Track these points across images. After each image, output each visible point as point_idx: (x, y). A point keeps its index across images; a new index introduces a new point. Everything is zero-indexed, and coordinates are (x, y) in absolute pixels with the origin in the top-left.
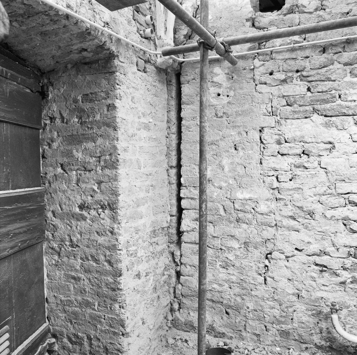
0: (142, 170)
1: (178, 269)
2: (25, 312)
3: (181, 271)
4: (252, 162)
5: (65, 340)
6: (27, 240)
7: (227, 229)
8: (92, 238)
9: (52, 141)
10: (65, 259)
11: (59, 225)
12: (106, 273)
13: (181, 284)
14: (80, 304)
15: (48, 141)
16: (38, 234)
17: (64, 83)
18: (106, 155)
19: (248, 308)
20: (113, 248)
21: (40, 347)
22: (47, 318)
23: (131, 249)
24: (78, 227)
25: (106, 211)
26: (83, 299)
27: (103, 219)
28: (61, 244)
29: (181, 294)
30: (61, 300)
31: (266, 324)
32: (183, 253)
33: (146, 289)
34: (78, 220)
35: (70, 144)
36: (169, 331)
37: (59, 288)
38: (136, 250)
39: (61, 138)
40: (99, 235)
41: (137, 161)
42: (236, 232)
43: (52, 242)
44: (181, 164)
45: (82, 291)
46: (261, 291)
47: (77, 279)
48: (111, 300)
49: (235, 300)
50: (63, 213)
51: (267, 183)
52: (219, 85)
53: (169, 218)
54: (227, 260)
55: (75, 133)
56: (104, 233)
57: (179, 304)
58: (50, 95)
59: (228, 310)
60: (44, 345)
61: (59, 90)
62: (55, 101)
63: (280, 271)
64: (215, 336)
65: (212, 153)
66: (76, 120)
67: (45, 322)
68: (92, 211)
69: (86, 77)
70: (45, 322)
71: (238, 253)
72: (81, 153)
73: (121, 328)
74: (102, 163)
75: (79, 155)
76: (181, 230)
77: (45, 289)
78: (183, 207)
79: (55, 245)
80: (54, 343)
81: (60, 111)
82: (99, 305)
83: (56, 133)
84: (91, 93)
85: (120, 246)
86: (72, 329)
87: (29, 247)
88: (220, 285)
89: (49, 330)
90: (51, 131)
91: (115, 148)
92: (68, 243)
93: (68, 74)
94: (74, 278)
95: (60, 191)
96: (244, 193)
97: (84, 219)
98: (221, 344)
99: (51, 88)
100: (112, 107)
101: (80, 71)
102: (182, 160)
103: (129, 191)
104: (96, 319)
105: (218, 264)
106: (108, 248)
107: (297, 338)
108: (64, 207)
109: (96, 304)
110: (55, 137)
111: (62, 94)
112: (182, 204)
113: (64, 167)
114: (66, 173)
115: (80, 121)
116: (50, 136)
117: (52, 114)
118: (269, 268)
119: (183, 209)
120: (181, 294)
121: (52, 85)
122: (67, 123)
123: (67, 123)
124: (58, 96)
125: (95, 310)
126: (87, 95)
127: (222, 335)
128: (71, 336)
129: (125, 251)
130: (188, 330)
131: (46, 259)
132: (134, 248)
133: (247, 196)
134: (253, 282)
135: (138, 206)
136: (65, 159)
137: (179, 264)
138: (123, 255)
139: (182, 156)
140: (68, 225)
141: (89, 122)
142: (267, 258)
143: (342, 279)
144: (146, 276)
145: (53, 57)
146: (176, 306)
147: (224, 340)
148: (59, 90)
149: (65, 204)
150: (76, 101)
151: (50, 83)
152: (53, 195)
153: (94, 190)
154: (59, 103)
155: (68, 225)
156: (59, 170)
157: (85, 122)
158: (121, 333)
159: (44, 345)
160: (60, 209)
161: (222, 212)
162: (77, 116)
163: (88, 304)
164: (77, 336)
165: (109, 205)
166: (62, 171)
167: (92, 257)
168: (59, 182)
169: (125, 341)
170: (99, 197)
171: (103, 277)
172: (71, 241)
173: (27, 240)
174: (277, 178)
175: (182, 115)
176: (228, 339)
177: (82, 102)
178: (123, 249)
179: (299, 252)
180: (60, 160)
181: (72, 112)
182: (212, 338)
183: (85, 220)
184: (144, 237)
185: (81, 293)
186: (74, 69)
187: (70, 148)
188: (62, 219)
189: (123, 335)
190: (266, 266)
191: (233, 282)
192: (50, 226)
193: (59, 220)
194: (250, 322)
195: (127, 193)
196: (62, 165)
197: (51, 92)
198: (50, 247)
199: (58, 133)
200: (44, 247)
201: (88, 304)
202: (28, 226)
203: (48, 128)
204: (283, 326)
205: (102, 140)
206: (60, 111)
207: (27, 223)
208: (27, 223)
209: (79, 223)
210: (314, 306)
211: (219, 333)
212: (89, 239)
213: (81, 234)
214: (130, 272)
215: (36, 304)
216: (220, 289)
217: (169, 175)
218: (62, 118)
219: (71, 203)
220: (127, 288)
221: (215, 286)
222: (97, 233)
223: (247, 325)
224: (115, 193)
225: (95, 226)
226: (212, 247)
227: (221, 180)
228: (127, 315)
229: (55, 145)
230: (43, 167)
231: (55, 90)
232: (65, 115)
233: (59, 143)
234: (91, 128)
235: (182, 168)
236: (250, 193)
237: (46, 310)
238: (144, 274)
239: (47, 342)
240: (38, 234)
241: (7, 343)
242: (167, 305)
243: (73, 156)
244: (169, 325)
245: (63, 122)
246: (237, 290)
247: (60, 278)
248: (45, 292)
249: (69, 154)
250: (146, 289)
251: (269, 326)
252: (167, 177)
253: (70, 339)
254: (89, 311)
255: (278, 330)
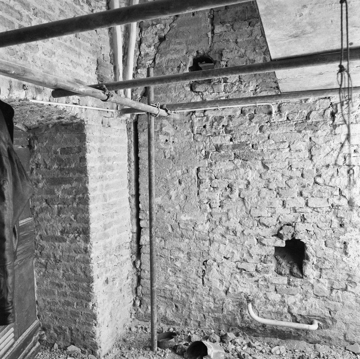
0: (108, 202)
1: (139, 274)
2: (23, 312)
3: (141, 275)
4: (192, 193)
5: (52, 332)
6: (23, 259)
7: (174, 243)
8: (71, 254)
9: (39, 183)
10: (51, 271)
11: (45, 245)
12: (83, 281)
13: (142, 286)
14: (63, 304)
15: (35, 182)
16: (30, 253)
17: (46, 138)
18: (79, 194)
19: (191, 302)
20: (88, 262)
21: (34, 338)
22: (38, 315)
23: (100, 262)
24: (60, 247)
25: (81, 236)
26: (65, 301)
27: (79, 241)
28: (47, 260)
29: (142, 293)
30: (48, 302)
31: (204, 313)
32: (142, 261)
33: (113, 291)
34: (60, 242)
35: (52, 184)
36: (133, 322)
37: (47, 292)
38: (105, 262)
39: (45, 180)
40: (76, 253)
41: (104, 196)
42: (182, 245)
43: (40, 258)
44: (140, 193)
45: (65, 295)
46: (200, 290)
47: (60, 286)
48: (86, 300)
49: (182, 296)
50: (49, 236)
51: (202, 209)
52: (167, 134)
53: (131, 234)
54: (175, 267)
55: (55, 177)
56: (80, 252)
57: (141, 301)
58: (36, 147)
59: (177, 304)
60: (37, 336)
61: (42, 143)
62: (39, 152)
63: (214, 275)
64: (168, 324)
65: (162, 185)
66: (56, 167)
67: (36, 319)
68: (71, 235)
69: (63, 135)
70: (36, 319)
71: (183, 261)
72: (61, 192)
73: (94, 321)
74: (77, 200)
75: (60, 194)
76: (140, 244)
77: (36, 294)
78: (142, 226)
79: (43, 261)
80: (43, 334)
81: (44, 160)
82: (77, 304)
83: (41, 176)
84: (68, 148)
85: (92, 261)
86: (57, 323)
87: (24, 264)
88: (171, 285)
89: (40, 325)
90: (37, 174)
91: (86, 189)
92: (52, 259)
93: (49, 132)
94: (58, 285)
95: (45, 220)
96: (187, 216)
97: (65, 241)
98: (171, 330)
99: (36, 141)
100: (83, 159)
101: (59, 131)
102: (140, 190)
103: (98, 219)
104: (74, 314)
105: (169, 270)
106: (83, 262)
107: (226, 322)
108: (49, 232)
109: (75, 304)
110: (40, 179)
111: (45, 147)
112: (140, 223)
113: (48, 201)
114: (50, 206)
115: (60, 167)
116: (36, 178)
117: (38, 162)
118: (206, 272)
119: (142, 228)
120: (142, 293)
121: (37, 139)
122: (49, 169)
123: (49, 169)
124: (41, 148)
125: (74, 308)
126: (64, 149)
127: (173, 323)
128: (57, 328)
129: (96, 264)
130: (147, 320)
131: (36, 271)
132: (103, 261)
133: (189, 218)
134: (194, 283)
135: (105, 229)
136: (49, 196)
137: (140, 270)
138: (94, 265)
139: (140, 187)
140: (53, 245)
141: (66, 169)
142: (204, 264)
143: (256, 279)
144: (112, 281)
145: (38, 121)
146: (138, 303)
147: (174, 327)
148: (42, 143)
149: (50, 230)
150: (56, 152)
151: (36, 137)
152: (40, 223)
153: (71, 220)
154: (43, 154)
155: (53, 245)
156: (44, 204)
157: (64, 169)
158: (94, 324)
159: (37, 336)
160: (45, 233)
161: (170, 230)
162: (57, 164)
163: (69, 304)
164: (60, 328)
165: (83, 230)
166: (46, 205)
167: (71, 269)
168: (44, 213)
169: (95, 328)
170: (75, 224)
171: (80, 283)
172: (55, 257)
173: (23, 259)
174: (210, 205)
175: (139, 155)
176: (177, 325)
177: (61, 154)
178: (94, 263)
179: (226, 260)
180: (45, 196)
181: (53, 161)
182: (166, 325)
183: (65, 242)
184: (110, 252)
185: (64, 296)
186: (54, 128)
187: (52, 187)
188: (47, 241)
189: (95, 325)
190: (204, 270)
191: (180, 283)
192: (38, 246)
193: (45, 242)
194: (193, 312)
195: (96, 221)
196: (46, 201)
197: (36, 145)
198: (38, 262)
199: (42, 176)
200: (34, 262)
201: (69, 304)
202: (23, 249)
203: (35, 172)
204: (216, 314)
205: (77, 183)
206: (44, 160)
207: (23, 247)
208: (23, 247)
209: (61, 244)
210: (237, 298)
211: (171, 322)
212: (69, 256)
213: (62, 251)
214: (100, 279)
215: (30, 306)
216: (171, 288)
217: (130, 202)
218: (46, 165)
219: (54, 229)
220: (98, 291)
221: (167, 286)
222: (75, 251)
223: (191, 314)
224: (87, 221)
225: (73, 246)
226: (164, 256)
227: (169, 206)
228: (98, 311)
229: (41, 185)
230: (31, 202)
231: (40, 144)
232: (48, 163)
233: (43, 184)
234: (68, 173)
235: (140, 196)
236: (190, 216)
237: (37, 310)
238: (112, 279)
239: (38, 334)
240: (30, 253)
241: (13, 335)
242: (131, 302)
243: (55, 194)
244: (133, 317)
245: (46, 168)
246: (183, 289)
247: (47, 285)
248: (36, 296)
249: (52, 192)
250: (113, 291)
251: (206, 314)
252: (128, 203)
253: (56, 331)
254: (70, 308)
255: (213, 318)
